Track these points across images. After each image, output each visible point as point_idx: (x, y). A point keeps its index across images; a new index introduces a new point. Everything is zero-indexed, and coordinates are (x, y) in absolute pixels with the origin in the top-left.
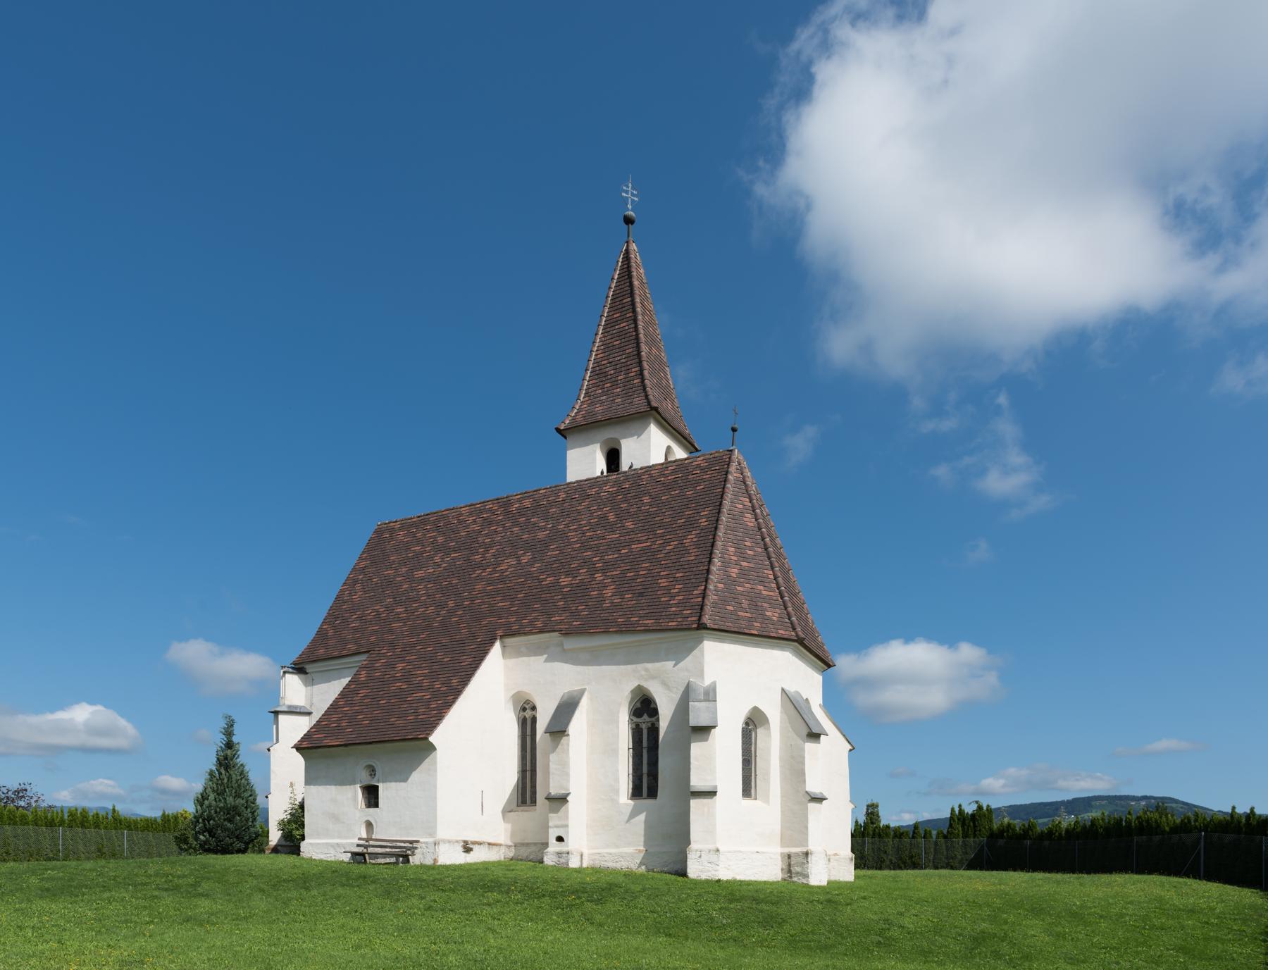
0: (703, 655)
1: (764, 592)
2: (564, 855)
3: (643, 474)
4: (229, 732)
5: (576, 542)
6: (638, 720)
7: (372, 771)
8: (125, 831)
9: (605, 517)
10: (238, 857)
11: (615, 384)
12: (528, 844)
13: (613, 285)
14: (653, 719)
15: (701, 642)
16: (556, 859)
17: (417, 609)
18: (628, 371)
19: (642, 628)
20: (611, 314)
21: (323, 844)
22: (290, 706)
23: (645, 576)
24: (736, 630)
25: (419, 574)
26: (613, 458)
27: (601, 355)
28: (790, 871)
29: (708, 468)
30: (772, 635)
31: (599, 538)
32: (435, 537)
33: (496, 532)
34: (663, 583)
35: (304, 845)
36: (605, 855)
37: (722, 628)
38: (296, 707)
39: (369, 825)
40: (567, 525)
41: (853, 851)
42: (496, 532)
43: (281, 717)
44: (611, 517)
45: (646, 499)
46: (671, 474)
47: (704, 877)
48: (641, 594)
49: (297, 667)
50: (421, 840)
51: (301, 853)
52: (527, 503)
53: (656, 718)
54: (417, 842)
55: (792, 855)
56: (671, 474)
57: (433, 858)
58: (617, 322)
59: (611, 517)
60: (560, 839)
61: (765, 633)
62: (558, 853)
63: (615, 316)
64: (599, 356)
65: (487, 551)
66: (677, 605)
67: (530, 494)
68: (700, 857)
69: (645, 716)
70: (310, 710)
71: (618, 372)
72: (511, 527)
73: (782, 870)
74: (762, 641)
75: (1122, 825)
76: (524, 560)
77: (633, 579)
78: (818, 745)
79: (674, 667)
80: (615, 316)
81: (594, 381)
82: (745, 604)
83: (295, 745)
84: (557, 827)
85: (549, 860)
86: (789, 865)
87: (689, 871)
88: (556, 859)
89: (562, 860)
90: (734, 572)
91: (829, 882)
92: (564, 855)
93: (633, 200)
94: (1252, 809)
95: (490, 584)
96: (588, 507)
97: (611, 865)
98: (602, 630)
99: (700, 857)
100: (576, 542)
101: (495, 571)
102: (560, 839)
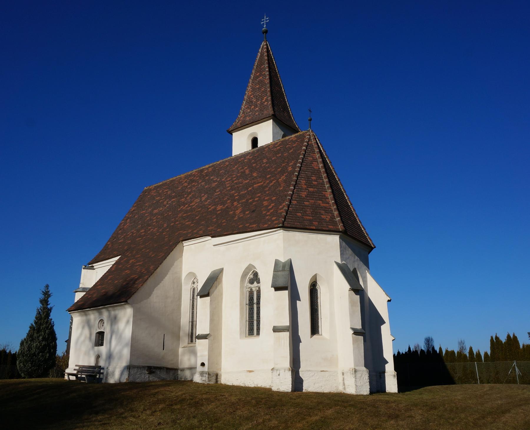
1: (322, 205)
3: (266, 148)
4: (45, 302)
5: (229, 187)
9: (244, 172)
17: (150, 229)
20: (256, 73)
23: (257, 201)
24: (302, 226)
25: (155, 211)
29: (296, 140)
30: (324, 229)
32: (167, 192)
33: (194, 186)
34: (265, 203)
37: (293, 226)
40: (227, 178)
42: (194, 186)
44: (247, 172)
45: (265, 161)
46: (278, 146)
48: (253, 211)
53: (311, 288)
55: (345, 373)
56: (278, 146)
58: (258, 77)
59: (247, 172)
61: (320, 228)
64: (249, 94)
65: (187, 197)
66: (270, 215)
68: (279, 375)
71: (257, 100)
72: (201, 183)
76: (203, 199)
77: (251, 203)
78: (274, 291)
79: (336, 262)
82: (309, 211)
83: (68, 309)
90: (304, 194)
93: (266, 18)
94: (428, 341)
95: (185, 214)
96: (237, 168)
100: (229, 187)
101: (189, 206)
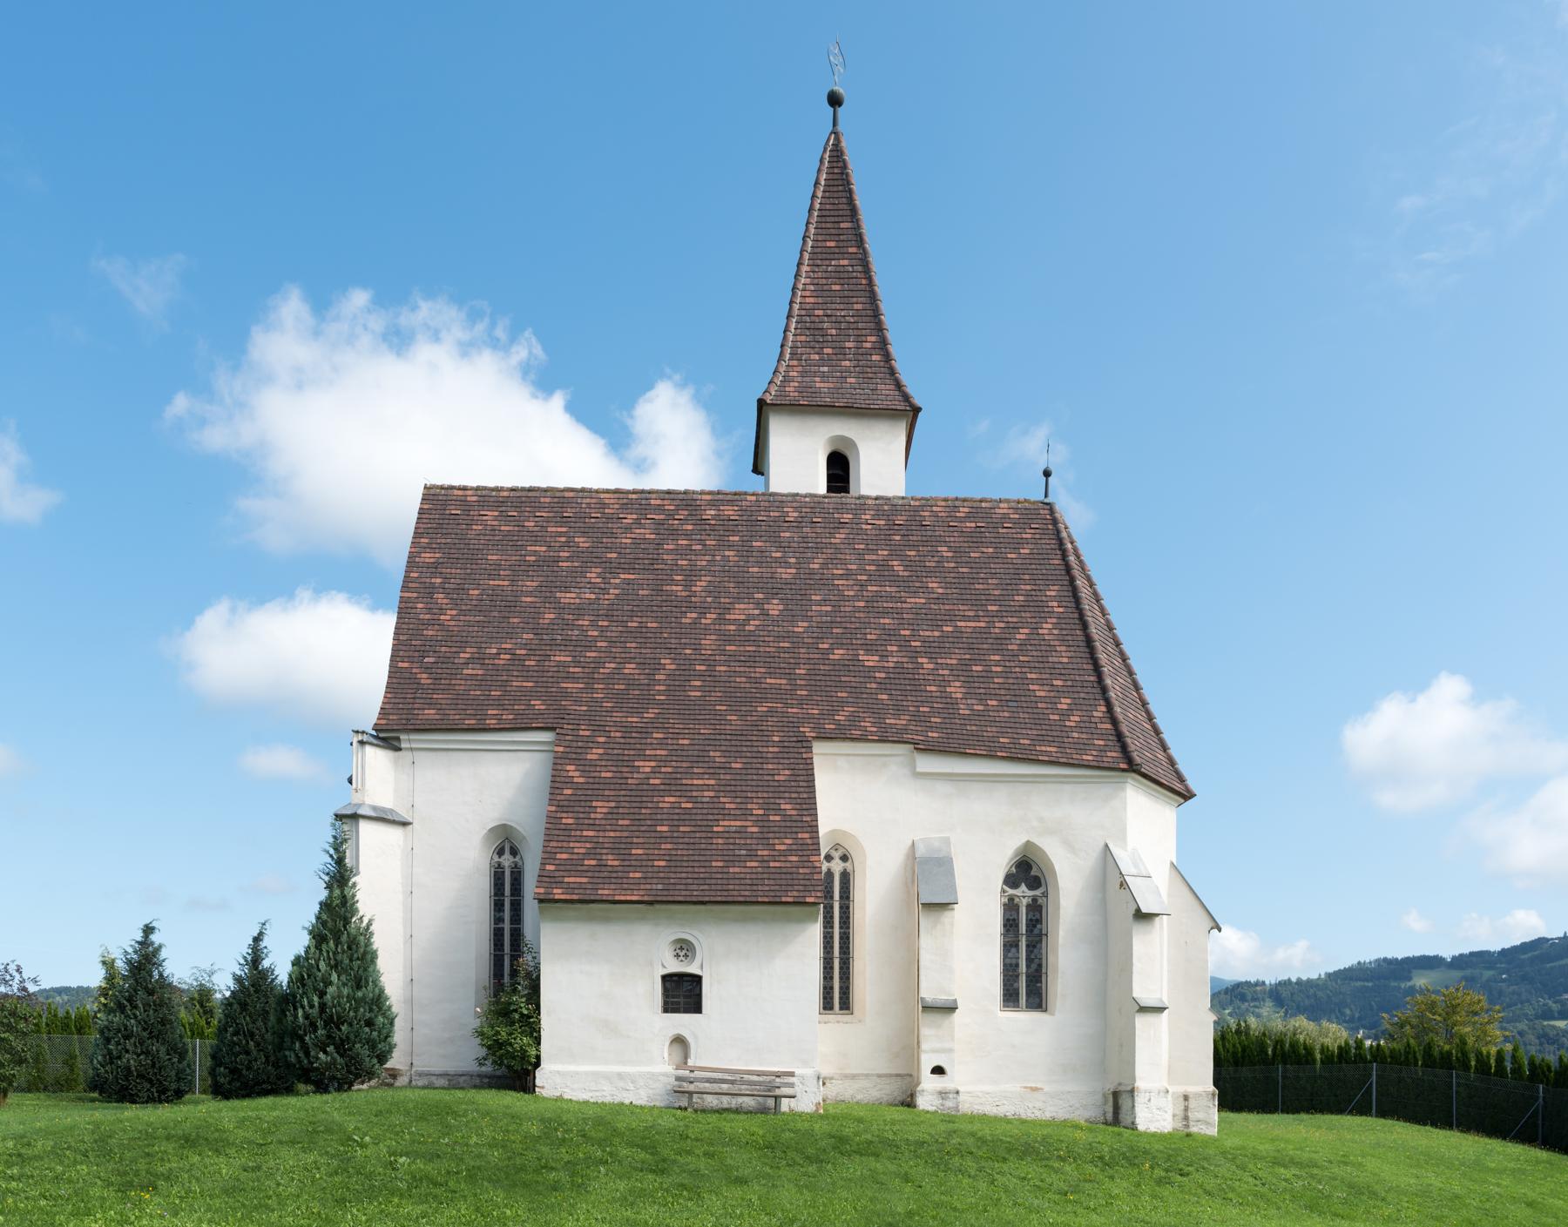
0: (1125, 809)
2: (951, 1096)
6: (1010, 891)
7: (684, 948)
8: (1541, 1086)
10: (1419, 1131)
11: (841, 352)
12: (854, 1077)
13: (820, 194)
14: (1038, 892)
15: (1124, 790)
16: (937, 1102)
18: (859, 340)
19: (1046, 758)
21: (586, 1073)
22: (375, 808)
26: (839, 468)
27: (812, 300)
28: (1186, 1118)
31: (891, 598)
35: (541, 1077)
36: (980, 1095)
38: (383, 810)
39: (680, 1041)
41: (1216, 1084)
43: (365, 828)
47: (1153, 1129)
49: (381, 735)
50: (798, 1072)
51: (537, 1089)
52: (729, 511)
54: (792, 1074)
57: (815, 1102)
60: (938, 1070)
62: (940, 1093)
63: (828, 244)
67: (729, 497)
68: (1149, 1100)
69: (1023, 887)
70: (407, 817)
73: (1174, 1116)
74: (1158, 792)
75: (1267, 1054)
80: (828, 244)
81: (803, 338)
84: (935, 1051)
85: (925, 1102)
86: (1186, 1109)
87: (1138, 1121)
88: (937, 1102)
89: (949, 1104)
91: (1174, 1129)
92: (951, 1096)
97: (991, 1110)
98: (985, 753)
99: (1149, 1100)
102: (938, 1070)
